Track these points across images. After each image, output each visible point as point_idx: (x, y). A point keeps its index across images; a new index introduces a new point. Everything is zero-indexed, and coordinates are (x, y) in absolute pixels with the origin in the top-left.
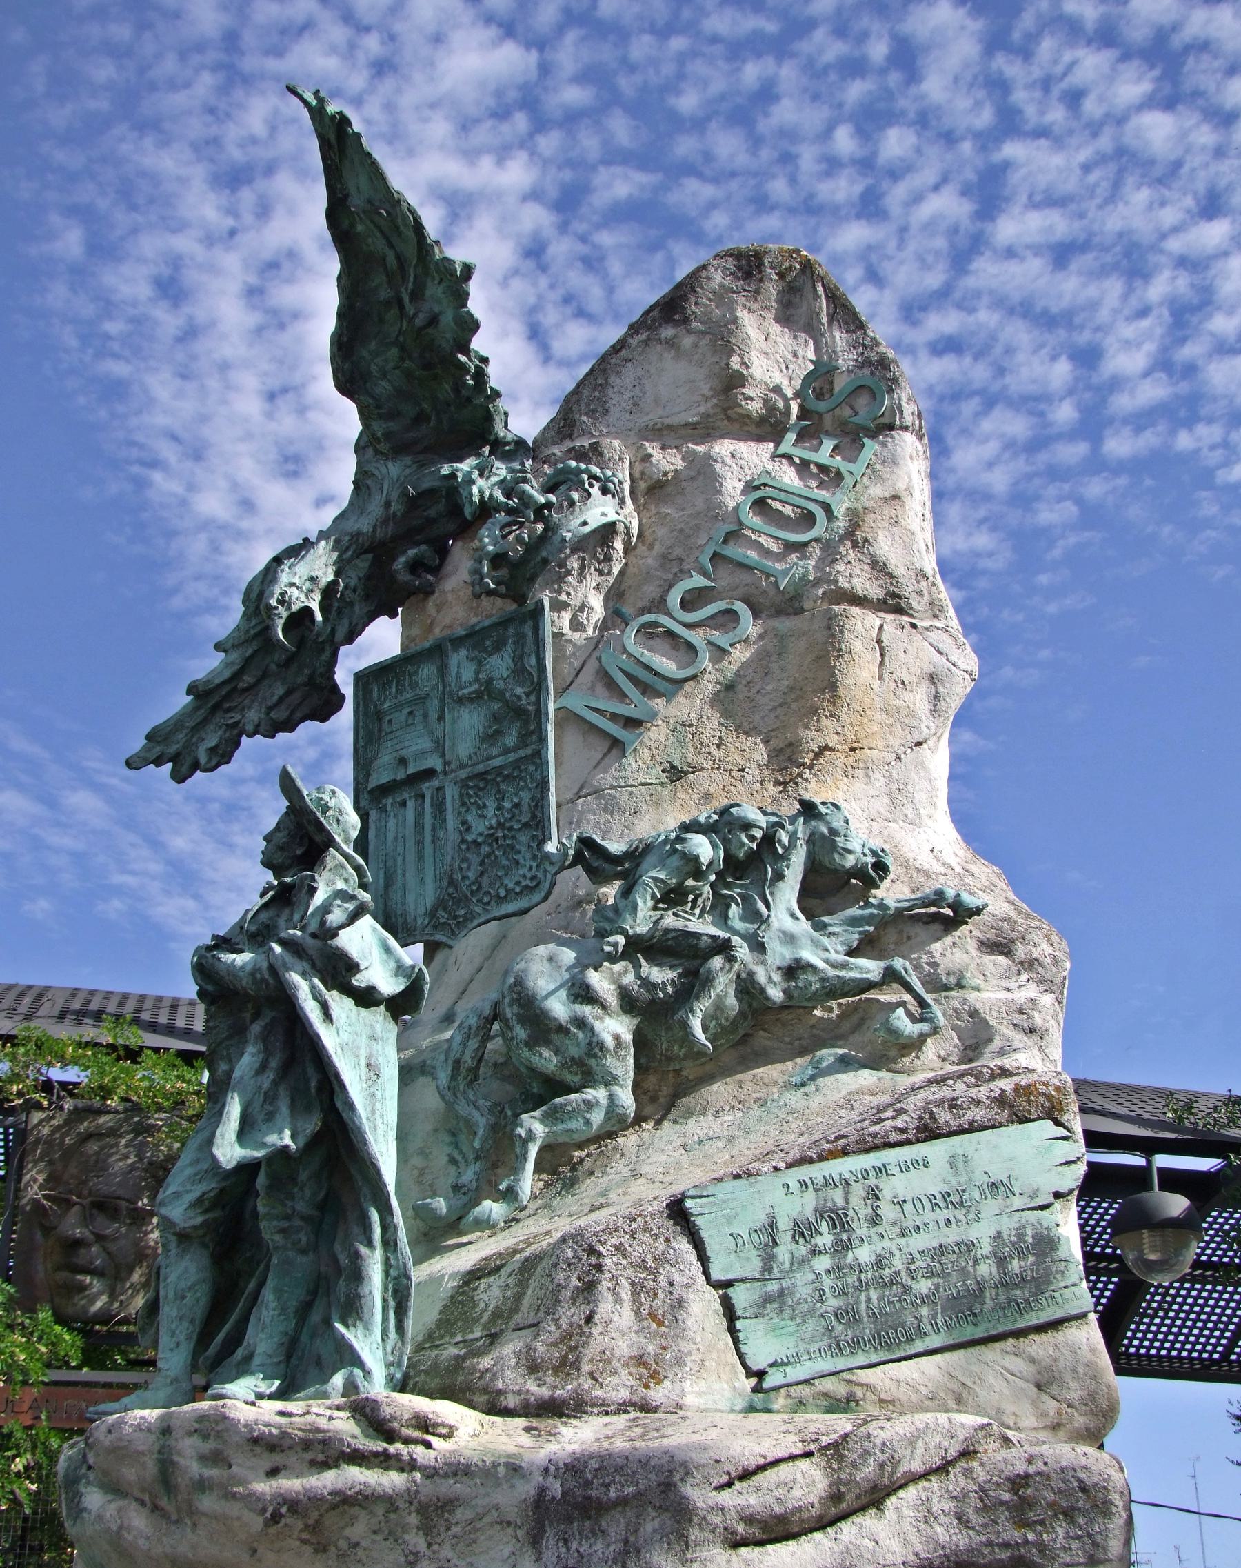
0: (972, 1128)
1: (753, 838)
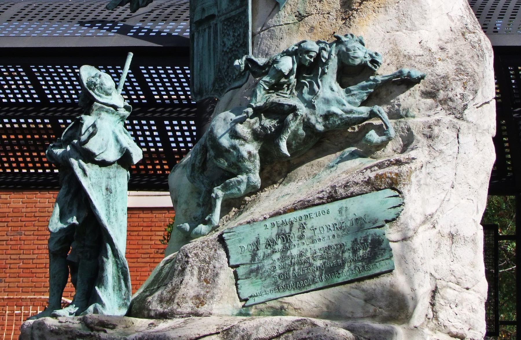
0: (352, 195)
1: (311, 57)
